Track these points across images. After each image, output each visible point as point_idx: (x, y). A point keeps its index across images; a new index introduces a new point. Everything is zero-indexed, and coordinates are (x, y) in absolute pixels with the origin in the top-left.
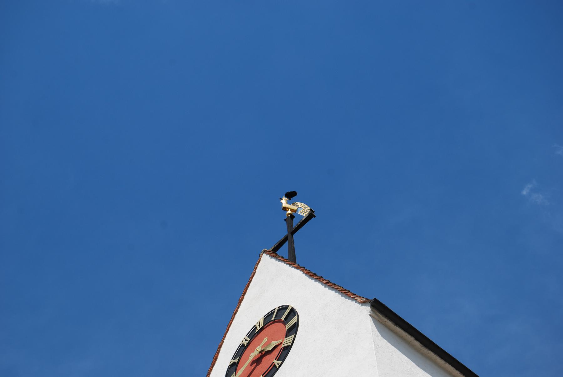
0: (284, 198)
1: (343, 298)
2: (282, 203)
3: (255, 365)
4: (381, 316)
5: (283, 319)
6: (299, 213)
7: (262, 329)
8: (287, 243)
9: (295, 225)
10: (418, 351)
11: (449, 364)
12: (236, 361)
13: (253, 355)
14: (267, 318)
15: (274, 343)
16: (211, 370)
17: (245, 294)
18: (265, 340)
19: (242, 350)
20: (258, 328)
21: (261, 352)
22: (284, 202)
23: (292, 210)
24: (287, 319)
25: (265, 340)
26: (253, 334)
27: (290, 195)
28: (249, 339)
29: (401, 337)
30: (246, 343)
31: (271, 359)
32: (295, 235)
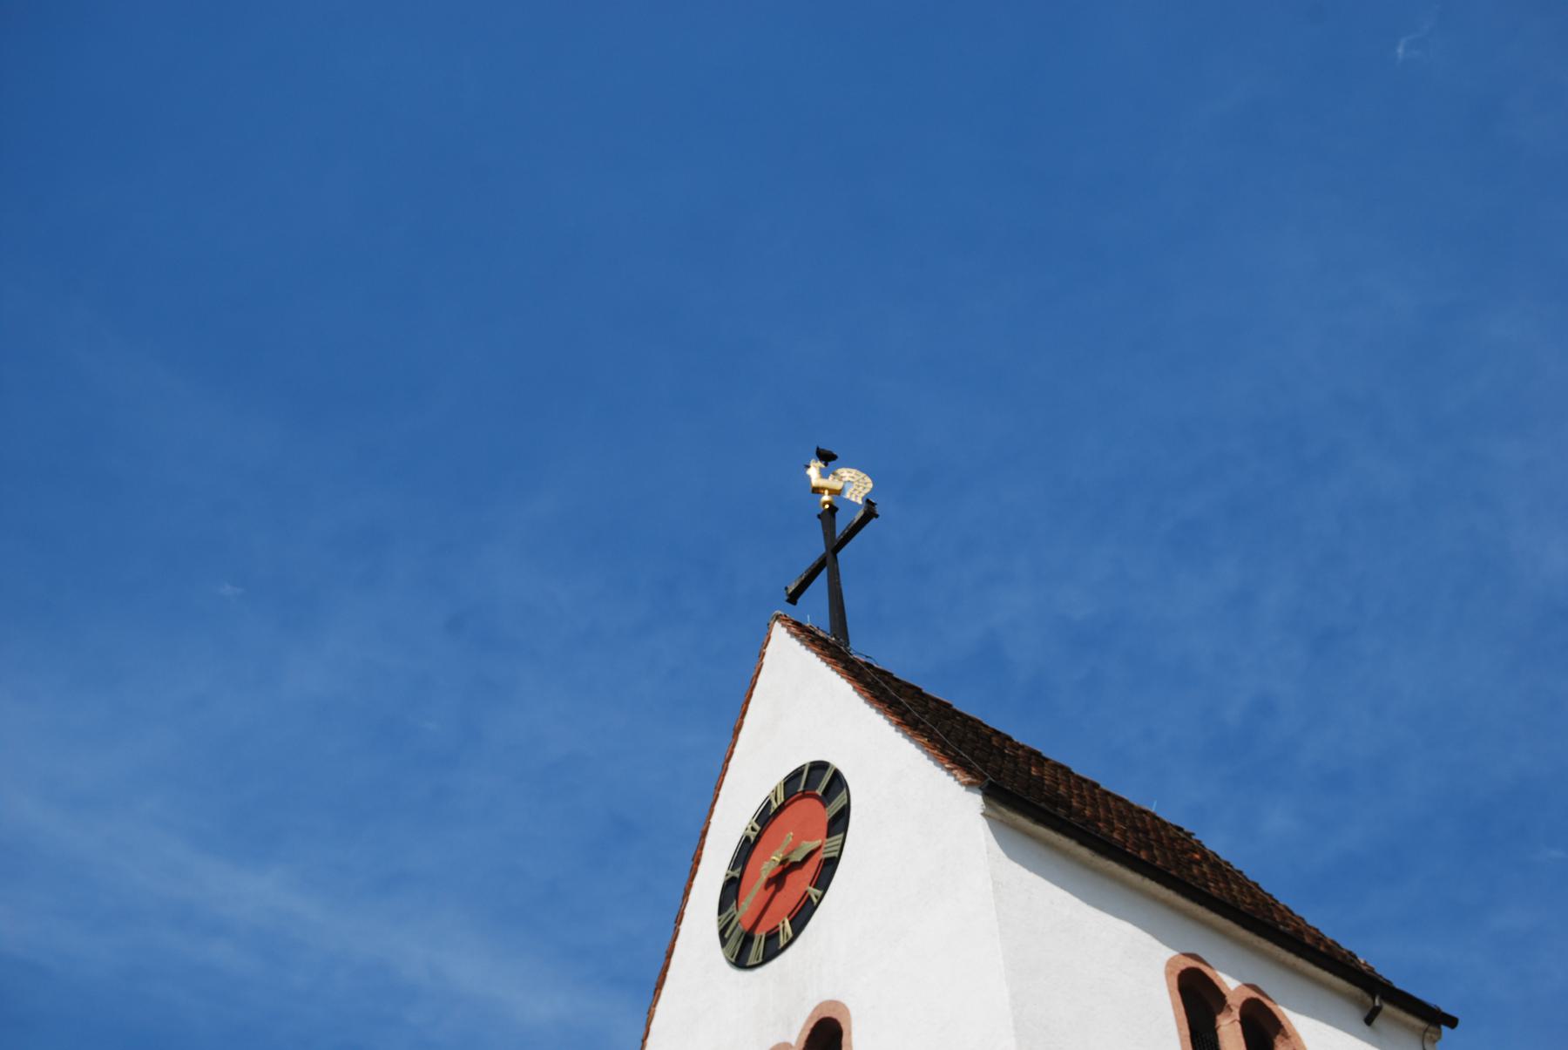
0: (812, 464)
1: (931, 763)
2: (809, 478)
3: (772, 888)
4: (1004, 810)
5: (819, 792)
6: (847, 496)
7: (781, 808)
8: (824, 572)
9: (839, 531)
10: (1086, 865)
11: (1152, 879)
12: (736, 874)
13: (766, 865)
14: (792, 780)
15: (809, 846)
16: (690, 886)
17: (744, 713)
18: (790, 836)
19: (746, 851)
20: (775, 805)
21: (783, 862)
22: (814, 472)
23: (832, 492)
24: (827, 797)
25: (790, 836)
26: (766, 817)
27: (826, 457)
28: (758, 828)
29: (1048, 844)
30: (753, 836)
31: (800, 883)
32: (840, 555)
